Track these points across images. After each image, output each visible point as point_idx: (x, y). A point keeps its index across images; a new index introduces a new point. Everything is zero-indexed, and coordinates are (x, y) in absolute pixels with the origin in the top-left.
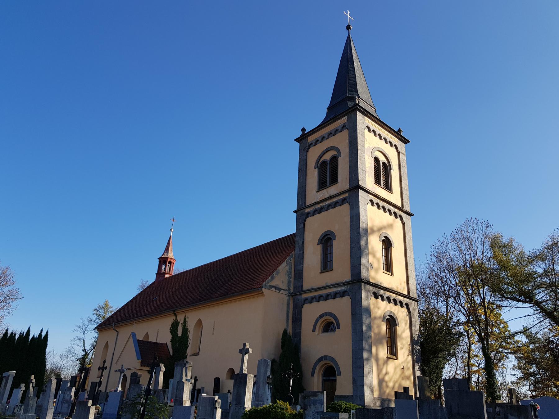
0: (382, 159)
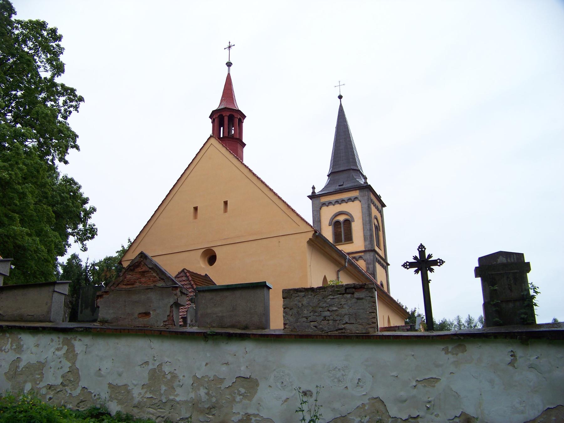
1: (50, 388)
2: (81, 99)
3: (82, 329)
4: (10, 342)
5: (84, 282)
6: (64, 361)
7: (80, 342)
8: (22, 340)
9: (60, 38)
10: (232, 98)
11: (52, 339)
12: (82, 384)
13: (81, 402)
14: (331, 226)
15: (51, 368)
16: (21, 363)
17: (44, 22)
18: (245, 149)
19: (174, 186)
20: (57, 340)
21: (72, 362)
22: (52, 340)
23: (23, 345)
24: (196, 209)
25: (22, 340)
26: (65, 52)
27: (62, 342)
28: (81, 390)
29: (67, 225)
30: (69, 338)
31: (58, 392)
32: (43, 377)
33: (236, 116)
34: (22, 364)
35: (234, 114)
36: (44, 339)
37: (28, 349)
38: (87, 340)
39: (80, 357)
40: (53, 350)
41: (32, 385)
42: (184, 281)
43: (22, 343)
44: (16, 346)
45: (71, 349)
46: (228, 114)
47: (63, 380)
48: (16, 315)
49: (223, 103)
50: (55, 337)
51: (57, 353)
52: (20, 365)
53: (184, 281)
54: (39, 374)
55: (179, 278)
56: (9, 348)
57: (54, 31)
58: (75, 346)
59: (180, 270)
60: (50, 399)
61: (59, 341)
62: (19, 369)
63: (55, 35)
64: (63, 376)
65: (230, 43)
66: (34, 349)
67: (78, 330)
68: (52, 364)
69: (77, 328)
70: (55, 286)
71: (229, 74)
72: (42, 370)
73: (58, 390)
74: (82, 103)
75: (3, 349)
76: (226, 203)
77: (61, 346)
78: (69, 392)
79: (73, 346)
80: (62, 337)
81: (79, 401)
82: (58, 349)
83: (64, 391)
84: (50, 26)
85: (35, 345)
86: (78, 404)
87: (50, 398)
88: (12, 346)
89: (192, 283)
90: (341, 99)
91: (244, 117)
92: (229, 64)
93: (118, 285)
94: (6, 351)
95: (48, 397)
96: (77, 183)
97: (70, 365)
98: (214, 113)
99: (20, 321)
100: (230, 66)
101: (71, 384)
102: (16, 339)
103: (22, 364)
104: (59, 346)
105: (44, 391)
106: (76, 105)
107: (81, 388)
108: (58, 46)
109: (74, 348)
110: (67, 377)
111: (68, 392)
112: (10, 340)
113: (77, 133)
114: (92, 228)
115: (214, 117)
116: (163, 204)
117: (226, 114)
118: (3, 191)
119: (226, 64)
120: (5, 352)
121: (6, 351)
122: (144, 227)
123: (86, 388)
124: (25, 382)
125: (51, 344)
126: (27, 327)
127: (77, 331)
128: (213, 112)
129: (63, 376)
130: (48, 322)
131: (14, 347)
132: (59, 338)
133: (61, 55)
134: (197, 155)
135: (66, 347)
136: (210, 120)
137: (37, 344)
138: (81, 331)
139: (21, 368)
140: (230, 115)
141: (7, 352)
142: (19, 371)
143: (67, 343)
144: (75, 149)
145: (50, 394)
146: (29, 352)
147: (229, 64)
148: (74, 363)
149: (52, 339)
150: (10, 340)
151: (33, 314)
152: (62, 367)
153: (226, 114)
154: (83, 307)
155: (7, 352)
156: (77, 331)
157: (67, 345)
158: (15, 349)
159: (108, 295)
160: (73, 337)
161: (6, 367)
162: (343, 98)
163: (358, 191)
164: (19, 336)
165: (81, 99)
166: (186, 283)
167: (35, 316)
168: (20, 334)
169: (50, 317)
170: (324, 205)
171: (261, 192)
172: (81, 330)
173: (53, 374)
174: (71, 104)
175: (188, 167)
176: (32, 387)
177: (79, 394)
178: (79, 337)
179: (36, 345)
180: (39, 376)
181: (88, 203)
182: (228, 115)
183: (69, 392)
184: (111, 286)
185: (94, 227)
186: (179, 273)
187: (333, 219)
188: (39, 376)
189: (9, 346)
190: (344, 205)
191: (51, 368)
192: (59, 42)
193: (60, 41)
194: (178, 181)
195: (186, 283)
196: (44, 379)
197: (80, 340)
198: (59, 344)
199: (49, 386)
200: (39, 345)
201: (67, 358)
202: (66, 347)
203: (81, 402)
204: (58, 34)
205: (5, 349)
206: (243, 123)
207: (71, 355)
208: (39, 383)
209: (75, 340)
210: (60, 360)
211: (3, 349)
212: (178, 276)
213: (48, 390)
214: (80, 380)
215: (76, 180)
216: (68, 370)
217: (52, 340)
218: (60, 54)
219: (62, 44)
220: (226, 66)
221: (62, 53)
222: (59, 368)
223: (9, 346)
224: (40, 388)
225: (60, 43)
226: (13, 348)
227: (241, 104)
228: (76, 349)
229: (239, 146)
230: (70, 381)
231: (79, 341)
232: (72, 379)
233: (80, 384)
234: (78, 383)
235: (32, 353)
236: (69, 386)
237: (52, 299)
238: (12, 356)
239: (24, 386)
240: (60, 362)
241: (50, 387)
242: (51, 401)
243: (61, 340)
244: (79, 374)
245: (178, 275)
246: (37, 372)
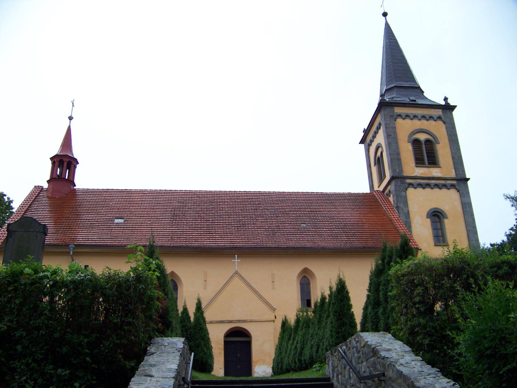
0: (422, 137)
5: (416, 318)
14: (363, 145)
18: (78, 166)
29: (500, 373)
35: (71, 160)
46: (68, 160)
71: (386, 21)
90: (387, 17)
91: (78, 163)
92: (71, 118)
98: (56, 156)
100: (71, 119)
118: (491, 274)
119: (69, 117)
136: (50, 162)
140: (69, 161)
147: (71, 118)
162: (388, 15)
163: (440, 110)
170: (431, 119)
187: (414, 134)
190: (432, 122)
206: (76, 168)
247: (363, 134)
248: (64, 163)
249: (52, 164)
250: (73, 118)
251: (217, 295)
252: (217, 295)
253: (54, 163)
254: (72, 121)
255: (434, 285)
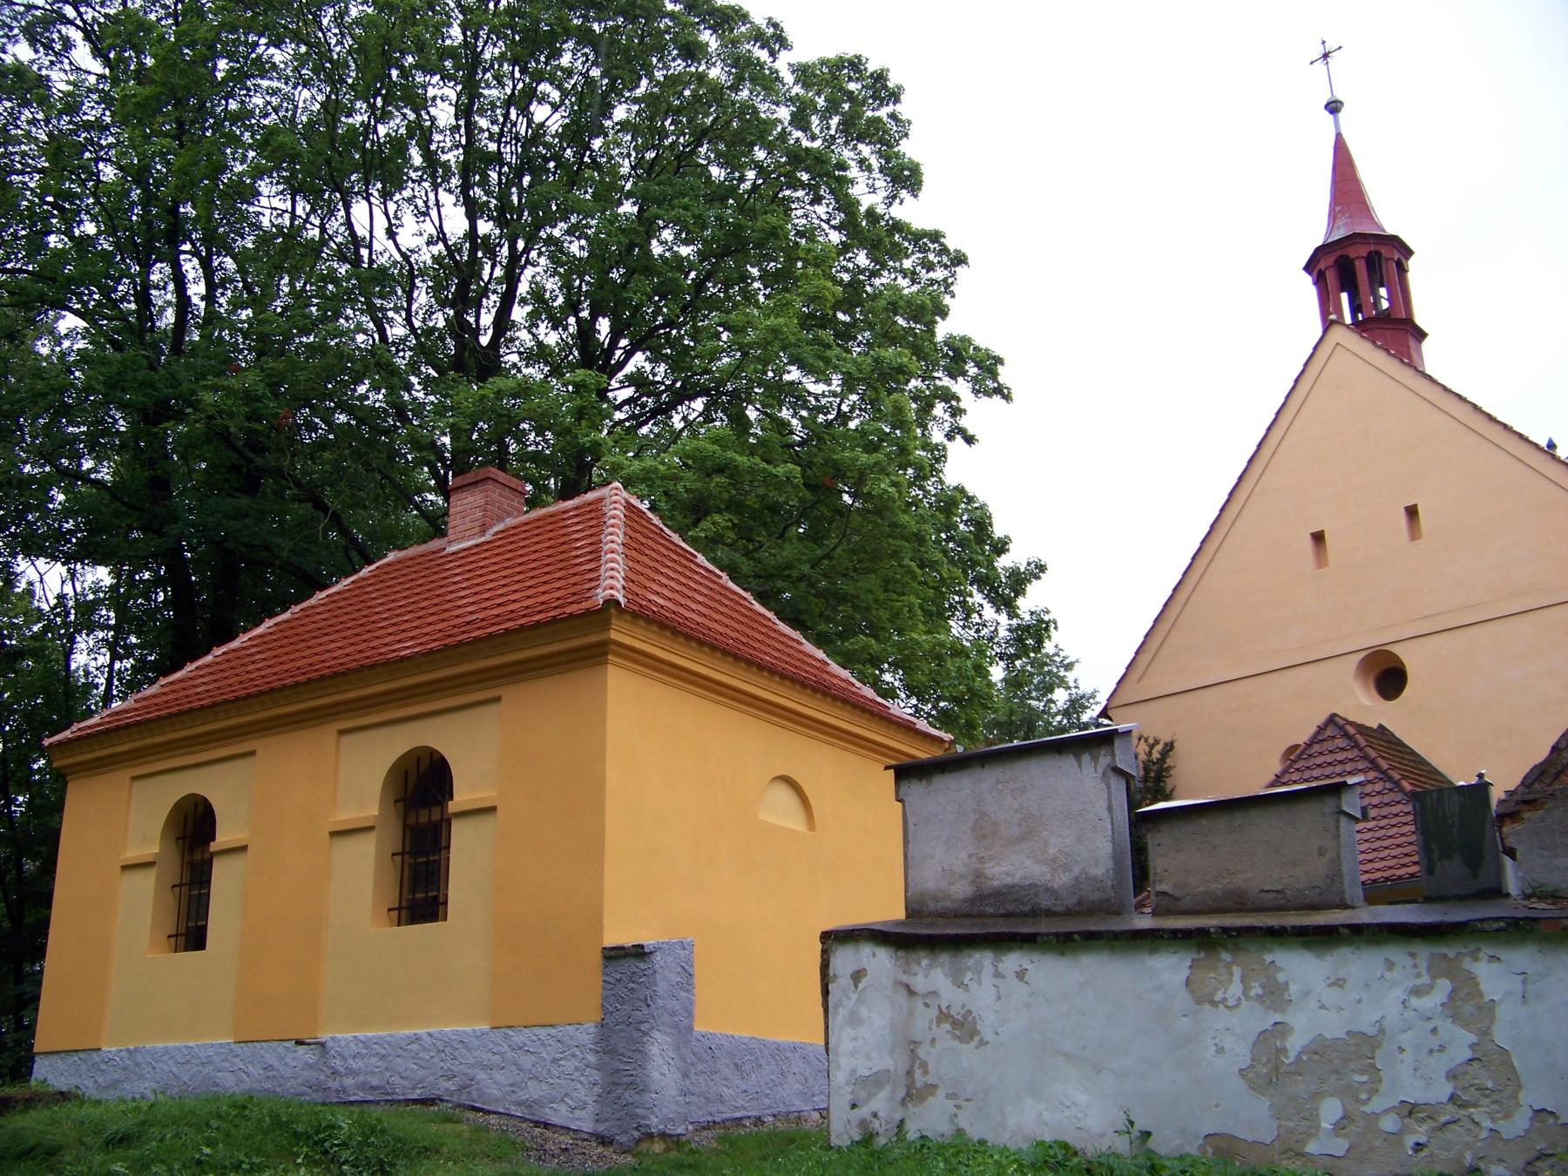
1: (1410, 1113)
2: (960, 260)
3: (1502, 924)
4: (1236, 977)
6: (1449, 1029)
7: (1494, 966)
8: (1281, 969)
9: (895, 96)
10: (1364, 203)
11: (1387, 960)
12: (1532, 1097)
13: (1538, 1158)
15: (1401, 1050)
16: (1290, 1039)
17: (858, 57)
18: (1412, 264)
19: (1241, 478)
20: (1409, 961)
21: (1479, 1029)
22: (1390, 965)
23: (1287, 983)
24: (1318, 538)
25: (1281, 969)
26: (913, 131)
27: (1429, 969)
28: (1531, 1119)
30: (1451, 952)
31: (1446, 1124)
32: (1380, 1081)
33: (1352, 256)
34: (1295, 1043)
35: (1344, 252)
36: (1360, 963)
37: (1306, 994)
38: (1522, 957)
39: (1503, 1013)
40: (1398, 993)
41: (1343, 1105)
42: (1342, 749)
43: (1281, 977)
44: (1263, 986)
45: (1465, 989)
46: (1363, 251)
47: (1455, 1087)
48: (1219, 893)
49: (1339, 223)
50: (1397, 953)
51: (1415, 1002)
52: (1288, 1046)
53: (1342, 749)
54: (1362, 1072)
55: (1325, 744)
56: (1239, 993)
57: (880, 77)
58: (1480, 979)
59: (1321, 719)
60: (1418, 1147)
61: (1415, 966)
62: (1287, 1058)
63: (881, 88)
64: (1452, 1076)
65: (1323, 42)
66: (1330, 996)
67: (1486, 926)
68: (1405, 1038)
69: (1481, 920)
70: (1340, 798)
71: (1339, 137)
72: (1373, 1058)
73: (1443, 1119)
74: (960, 270)
75: (1218, 997)
76: (1412, 512)
77: (1425, 979)
78: (1487, 1124)
79: (1472, 979)
80: (1424, 952)
81: (1534, 1154)
82: (1417, 991)
83: (1467, 1124)
84: (872, 67)
85: (1329, 982)
86: (1529, 1163)
87: (1418, 1144)
88: (1246, 989)
89: (1373, 754)
91: (1408, 252)
92: (1334, 107)
93: (1557, 775)
94: (1231, 1002)
95: (1410, 1140)
96: (973, 497)
97: (1473, 1038)
98: (1319, 252)
99: (1238, 911)
101: (1488, 1100)
102: (1256, 967)
103: (1295, 1043)
104: (1419, 982)
105: (1389, 1124)
106: (945, 280)
107: (1530, 1114)
108: (893, 116)
109: (1478, 984)
110: (1468, 1077)
111: (1484, 1125)
112: (1237, 971)
113: (997, 351)
114: (1042, 621)
115: (1322, 265)
116: (1214, 533)
117: (1358, 252)
119: (1326, 107)
120: (1227, 1007)
121: (1231, 1002)
122: (1166, 605)
123: (1552, 1113)
124: (1317, 1096)
125: (1388, 975)
126: (1293, 927)
127: (1483, 931)
128: (1318, 251)
129: (1452, 1076)
130: (1338, 907)
131: (1257, 990)
132: (1413, 955)
133: (904, 142)
134: (1297, 381)
135: (1444, 986)
136: (1308, 280)
137: (1339, 979)
138: (1497, 930)
139: (1292, 1055)
141: (1235, 1006)
142: (1289, 1065)
143: (1448, 969)
144: (997, 399)
145: (1415, 1132)
146: (1313, 1004)
147: (1334, 107)
148: (1485, 1033)
149: (1387, 960)
150: (1237, 971)
151: (1279, 887)
152: (1442, 1048)
153: (1358, 252)
154: (1436, 855)
155: (1235, 1006)
156: (1483, 931)
157: (1450, 976)
158: (1260, 998)
159: (1541, 812)
160: (1464, 950)
161: (1241, 1054)
164: (1268, 958)
165: (960, 260)
166: (1350, 755)
167: (1288, 892)
168: (1270, 951)
169: (1343, 892)
171: (1521, 467)
172: (1495, 926)
173: (1416, 1069)
174: (932, 275)
175: (1275, 420)
176: (1345, 1109)
177: (1526, 1131)
178: (1488, 950)
179: (1333, 980)
180: (1365, 1078)
181: (1008, 550)
182: (1365, 254)
183: (1487, 1124)
184: (1532, 784)
185: (1046, 618)
186: (1321, 729)
188: (1365, 1078)
189: (1235, 989)
191: (1401, 1050)
192: (894, 104)
193: (897, 101)
194: (1250, 461)
195: (1350, 755)
196: (1384, 1086)
197: (1493, 958)
198: (1419, 975)
199: (1409, 1107)
200: (1344, 980)
201: (1456, 1018)
202: (1444, 986)
203: (1538, 1158)
204: (890, 85)
205: (1225, 999)
206: (1407, 271)
207: (1468, 1008)
208: (1369, 1099)
209: (1476, 959)
210: (1431, 1025)
211: (1218, 997)
212: (1320, 738)
213: (1406, 1121)
214: (1520, 1086)
215: (971, 490)
216: (1468, 1054)
217: (1390, 965)
218: (900, 138)
219: (904, 109)
220: (1327, 113)
221: (906, 135)
222: (1431, 1051)
223: (1235, 989)
224: (1376, 1116)
225: (898, 108)
226: (1252, 993)
227: (1390, 219)
228: (1483, 987)
229: (1412, 343)
230: (1481, 1089)
231: (1489, 961)
232: (1490, 1084)
233: (1524, 1097)
234: (1514, 1096)
235: (1323, 1007)
236: (1481, 1106)
237: (1339, 836)
238: (1253, 1020)
239: (1317, 1109)
240: (1434, 1030)
241: (1410, 1110)
242: (1422, 1154)
243: (1423, 962)
244: (1514, 1068)
245: (1317, 733)
246: (1352, 1066)
247: (1375, 726)
248: (1353, 264)
249: (1315, 284)
250: (1341, 103)
251: (827, 1028)
252: (827, 1028)
253: (1320, 281)
254: (1341, 115)
255: (96, 604)
